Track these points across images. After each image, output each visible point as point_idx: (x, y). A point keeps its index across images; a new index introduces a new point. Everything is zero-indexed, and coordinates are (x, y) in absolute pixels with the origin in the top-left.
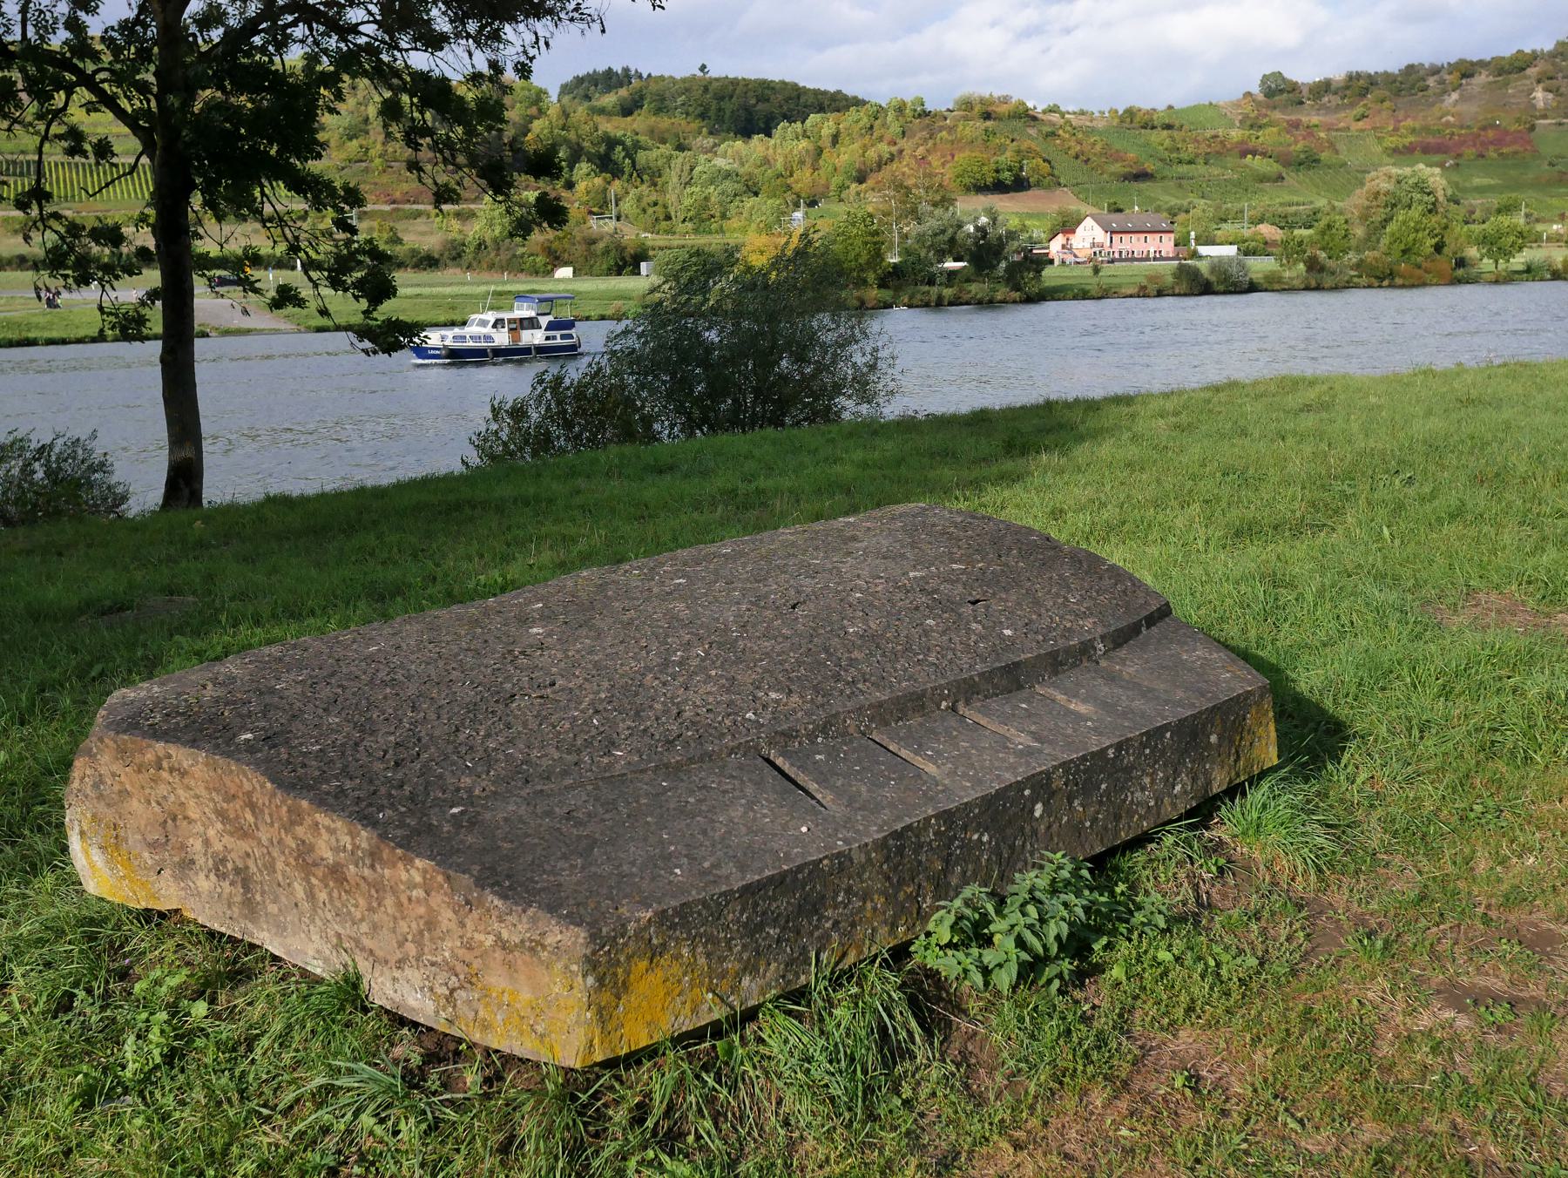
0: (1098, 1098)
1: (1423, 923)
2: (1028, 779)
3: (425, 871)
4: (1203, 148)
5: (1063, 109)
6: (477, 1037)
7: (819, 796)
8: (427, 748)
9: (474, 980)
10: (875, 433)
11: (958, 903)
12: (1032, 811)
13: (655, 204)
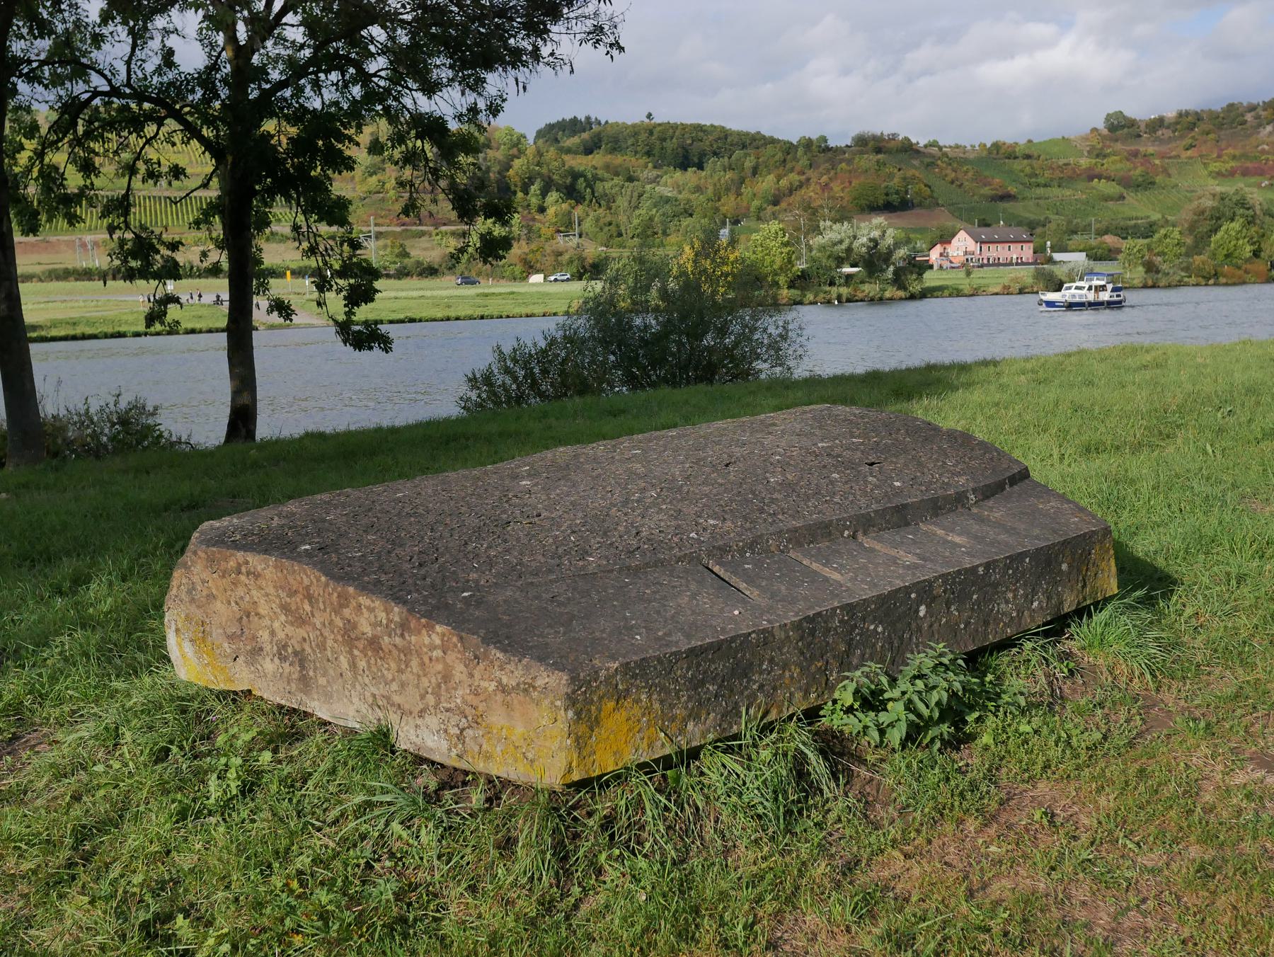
0: (972, 825)
1: (1239, 712)
2: (914, 584)
3: (444, 635)
4: (1058, 174)
5: (941, 144)
6: (480, 766)
7: (748, 593)
8: (443, 555)
9: (479, 720)
10: (787, 388)
11: (858, 673)
12: (917, 611)
13: (610, 224)
